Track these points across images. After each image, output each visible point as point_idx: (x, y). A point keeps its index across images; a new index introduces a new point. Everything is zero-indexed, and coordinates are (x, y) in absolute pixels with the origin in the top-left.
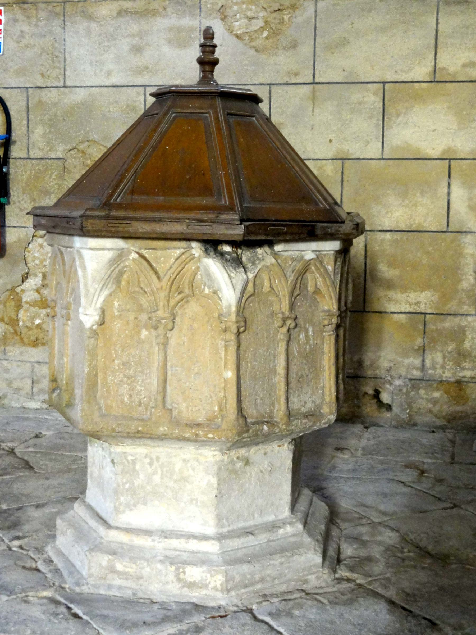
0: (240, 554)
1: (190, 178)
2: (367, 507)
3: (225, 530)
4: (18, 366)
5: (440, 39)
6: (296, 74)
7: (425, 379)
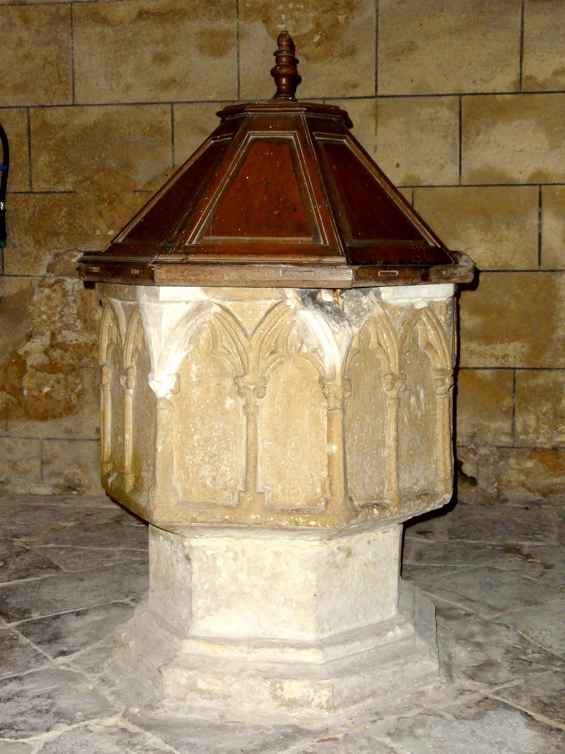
0: (346, 663)
1: (279, 214)
2: (473, 601)
3: (326, 635)
4: (24, 444)
5: (527, 43)
6: (355, 86)
7: (515, 446)
